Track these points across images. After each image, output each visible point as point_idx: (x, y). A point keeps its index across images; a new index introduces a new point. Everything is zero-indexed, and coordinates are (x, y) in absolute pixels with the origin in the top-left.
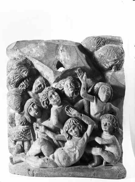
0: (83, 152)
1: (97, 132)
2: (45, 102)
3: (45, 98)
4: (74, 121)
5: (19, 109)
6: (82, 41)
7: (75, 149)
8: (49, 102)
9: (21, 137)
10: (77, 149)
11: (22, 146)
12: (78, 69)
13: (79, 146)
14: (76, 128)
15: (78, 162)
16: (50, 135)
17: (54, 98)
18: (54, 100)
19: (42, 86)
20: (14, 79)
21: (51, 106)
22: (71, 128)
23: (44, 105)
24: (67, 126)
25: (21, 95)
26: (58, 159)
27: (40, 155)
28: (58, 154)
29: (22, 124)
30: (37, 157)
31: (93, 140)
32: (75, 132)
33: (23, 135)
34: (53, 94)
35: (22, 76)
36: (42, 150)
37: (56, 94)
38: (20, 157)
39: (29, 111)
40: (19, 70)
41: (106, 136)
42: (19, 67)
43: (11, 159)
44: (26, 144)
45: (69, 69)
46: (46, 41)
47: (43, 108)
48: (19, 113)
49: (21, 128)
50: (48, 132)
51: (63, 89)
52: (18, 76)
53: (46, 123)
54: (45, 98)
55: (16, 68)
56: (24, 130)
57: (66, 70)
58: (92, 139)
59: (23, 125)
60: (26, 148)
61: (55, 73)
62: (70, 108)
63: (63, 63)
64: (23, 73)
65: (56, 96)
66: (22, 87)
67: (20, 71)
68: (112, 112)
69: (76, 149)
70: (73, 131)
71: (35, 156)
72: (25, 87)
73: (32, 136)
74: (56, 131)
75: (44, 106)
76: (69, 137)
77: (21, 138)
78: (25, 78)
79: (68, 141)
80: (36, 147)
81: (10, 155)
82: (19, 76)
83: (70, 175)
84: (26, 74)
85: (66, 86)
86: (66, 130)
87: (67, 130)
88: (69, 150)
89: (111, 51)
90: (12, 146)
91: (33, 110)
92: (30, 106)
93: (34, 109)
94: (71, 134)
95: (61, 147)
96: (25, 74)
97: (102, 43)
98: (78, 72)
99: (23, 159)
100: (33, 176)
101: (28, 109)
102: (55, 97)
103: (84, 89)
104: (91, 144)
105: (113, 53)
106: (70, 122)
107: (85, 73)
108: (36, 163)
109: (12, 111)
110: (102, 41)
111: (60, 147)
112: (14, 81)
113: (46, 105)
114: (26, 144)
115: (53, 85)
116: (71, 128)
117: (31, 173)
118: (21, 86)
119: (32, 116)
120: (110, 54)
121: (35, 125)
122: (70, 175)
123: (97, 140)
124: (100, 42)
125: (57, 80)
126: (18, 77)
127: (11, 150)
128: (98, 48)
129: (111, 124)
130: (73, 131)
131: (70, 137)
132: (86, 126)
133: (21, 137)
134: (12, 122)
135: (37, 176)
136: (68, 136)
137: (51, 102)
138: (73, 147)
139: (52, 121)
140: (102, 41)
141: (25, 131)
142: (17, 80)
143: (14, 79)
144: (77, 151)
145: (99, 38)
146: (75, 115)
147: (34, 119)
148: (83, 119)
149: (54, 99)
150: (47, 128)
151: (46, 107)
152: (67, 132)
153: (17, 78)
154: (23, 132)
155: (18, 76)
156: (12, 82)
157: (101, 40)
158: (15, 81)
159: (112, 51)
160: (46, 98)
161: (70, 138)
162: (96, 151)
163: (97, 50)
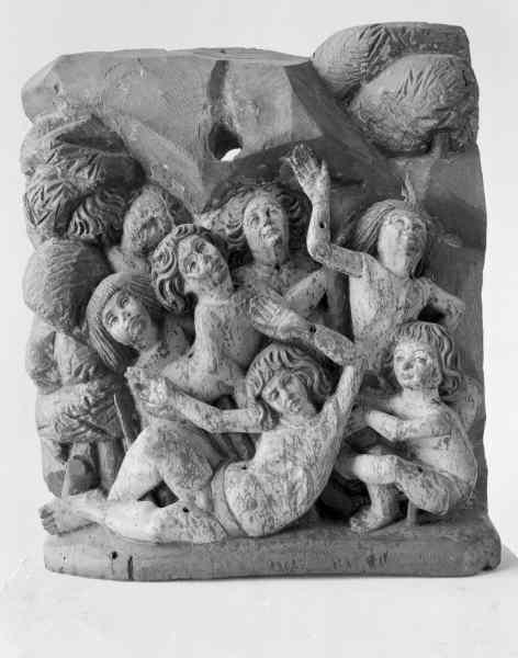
0: (326, 471)
1: (380, 385)
2: (167, 285)
3: (167, 270)
4: (284, 355)
5: (67, 314)
6: (313, 50)
7: (289, 465)
8: (182, 282)
9: (82, 429)
10: (298, 463)
11: (91, 461)
12: (296, 148)
13: (307, 451)
14: (296, 381)
15: (307, 515)
16: (194, 413)
17: (202, 267)
18: (199, 270)
19: (161, 226)
20: (42, 199)
21: (191, 301)
22: (275, 383)
23: (165, 298)
24: (257, 374)
25: (74, 261)
26: (229, 510)
27: (158, 495)
28: (233, 487)
29: (81, 376)
30: (148, 503)
31: (363, 426)
32: (291, 396)
33: (90, 420)
34: (199, 249)
35: (75, 188)
36: (161, 472)
37: (210, 249)
38: (85, 505)
39: (104, 321)
40: (64, 161)
41: (415, 411)
42: (62, 151)
43: (46, 514)
44: (104, 450)
45: (259, 148)
46: (170, 52)
47: (163, 308)
48: (68, 332)
49: (77, 395)
50: (184, 404)
51: (241, 231)
52: (60, 187)
53: (174, 371)
54: (167, 270)
55: (50, 154)
56: (90, 400)
57: (247, 154)
58: (359, 425)
59: (87, 379)
60: (106, 470)
61: (206, 170)
62: (270, 303)
63: (238, 128)
64: (80, 174)
65: (207, 259)
66: (82, 231)
67: (68, 167)
68: (431, 315)
69: (295, 464)
70: (283, 395)
71: (142, 499)
72: (91, 229)
73: (122, 422)
74: (224, 400)
75: (168, 300)
76: (265, 418)
77: (82, 433)
78: (90, 194)
79: (265, 434)
80: (138, 465)
81: (48, 498)
82: (65, 187)
83: (277, 568)
84: (92, 177)
85: (257, 220)
86: (254, 391)
87: (257, 392)
88: (270, 468)
89: (424, 77)
90: (58, 466)
91: (121, 318)
92: (110, 302)
93: (124, 314)
94: (275, 405)
95: (242, 460)
96: (86, 179)
97: (387, 49)
98: (294, 160)
99: (95, 514)
100: (131, 578)
101: (100, 314)
102: (207, 262)
103: (322, 226)
104: (358, 441)
105: (431, 82)
106: (268, 359)
107: (323, 162)
108: (133, 521)
109: (45, 329)
110: (391, 43)
111: (239, 458)
112: (44, 206)
113: (171, 297)
114: (104, 450)
115: (204, 222)
116: (275, 383)
117: (121, 564)
118: (76, 229)
119: (120, 344)
120: (421, 86)
121: (133, 374)
122: (277, 568)
123: (379, 421)
124: (381, 46)
125: (220, 198)
126: (60, 192)
127: (54, 481)
128: (373, 68)
129: (429, 361)
130: (283, 395)
131: (273, 417)
132: (333, 371)
133: (82, 429)
134: (45, 372)
135: (144, 580)
136: (261, 416)
137: (191, 286)
138: (284, 457)
139: (200, 365)
140: (387, 42)
141: (95, 406)
142: (55, 204)
143: (46, 198)
144: (300, 473)
145: (375, 28)
146: (289, 329)
147: (128, 354)
148: (317, 344)
149: (201, 272)
150: (173, 389)
151: (174, 303)
152: (259, 398)
153: (56, 197)
154: (86, 407)
155: (60, 187)
156: (40, 213)
157: (385, 38)
158: (47, 207)
159: (428, 78)
160: (170, 267)
161: (270, 420)
162: (371, 468)
163: (370, 78)
